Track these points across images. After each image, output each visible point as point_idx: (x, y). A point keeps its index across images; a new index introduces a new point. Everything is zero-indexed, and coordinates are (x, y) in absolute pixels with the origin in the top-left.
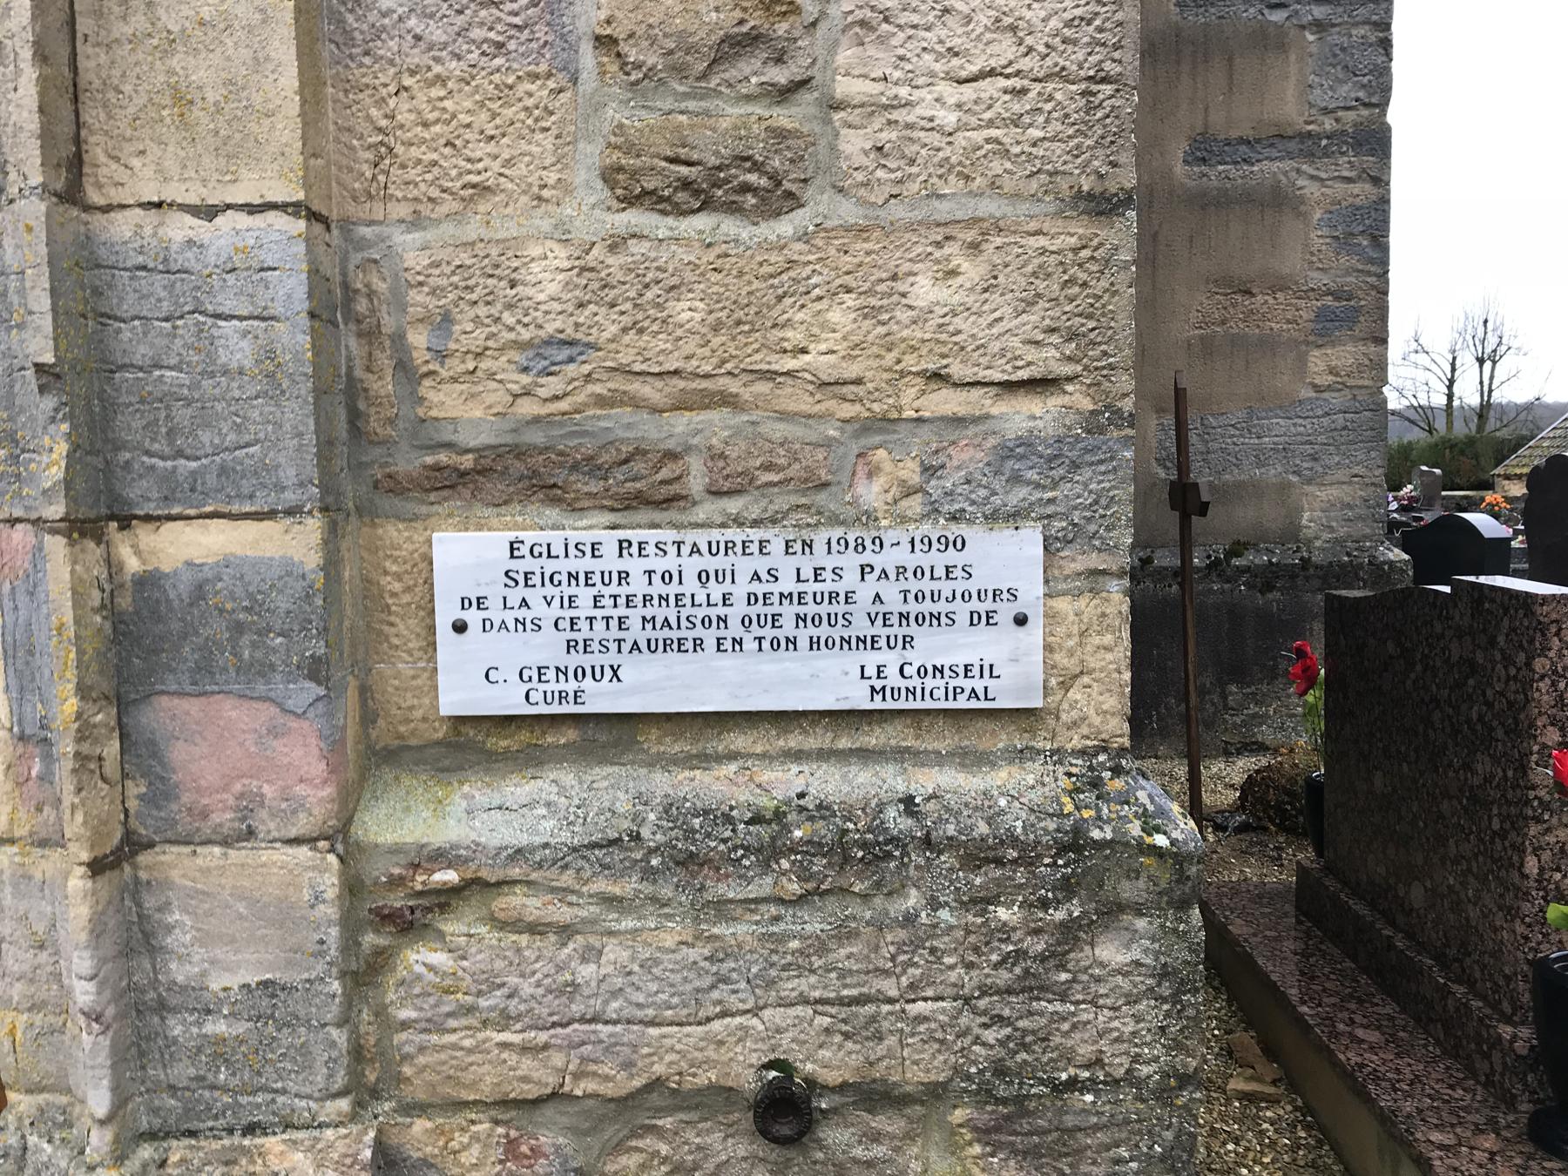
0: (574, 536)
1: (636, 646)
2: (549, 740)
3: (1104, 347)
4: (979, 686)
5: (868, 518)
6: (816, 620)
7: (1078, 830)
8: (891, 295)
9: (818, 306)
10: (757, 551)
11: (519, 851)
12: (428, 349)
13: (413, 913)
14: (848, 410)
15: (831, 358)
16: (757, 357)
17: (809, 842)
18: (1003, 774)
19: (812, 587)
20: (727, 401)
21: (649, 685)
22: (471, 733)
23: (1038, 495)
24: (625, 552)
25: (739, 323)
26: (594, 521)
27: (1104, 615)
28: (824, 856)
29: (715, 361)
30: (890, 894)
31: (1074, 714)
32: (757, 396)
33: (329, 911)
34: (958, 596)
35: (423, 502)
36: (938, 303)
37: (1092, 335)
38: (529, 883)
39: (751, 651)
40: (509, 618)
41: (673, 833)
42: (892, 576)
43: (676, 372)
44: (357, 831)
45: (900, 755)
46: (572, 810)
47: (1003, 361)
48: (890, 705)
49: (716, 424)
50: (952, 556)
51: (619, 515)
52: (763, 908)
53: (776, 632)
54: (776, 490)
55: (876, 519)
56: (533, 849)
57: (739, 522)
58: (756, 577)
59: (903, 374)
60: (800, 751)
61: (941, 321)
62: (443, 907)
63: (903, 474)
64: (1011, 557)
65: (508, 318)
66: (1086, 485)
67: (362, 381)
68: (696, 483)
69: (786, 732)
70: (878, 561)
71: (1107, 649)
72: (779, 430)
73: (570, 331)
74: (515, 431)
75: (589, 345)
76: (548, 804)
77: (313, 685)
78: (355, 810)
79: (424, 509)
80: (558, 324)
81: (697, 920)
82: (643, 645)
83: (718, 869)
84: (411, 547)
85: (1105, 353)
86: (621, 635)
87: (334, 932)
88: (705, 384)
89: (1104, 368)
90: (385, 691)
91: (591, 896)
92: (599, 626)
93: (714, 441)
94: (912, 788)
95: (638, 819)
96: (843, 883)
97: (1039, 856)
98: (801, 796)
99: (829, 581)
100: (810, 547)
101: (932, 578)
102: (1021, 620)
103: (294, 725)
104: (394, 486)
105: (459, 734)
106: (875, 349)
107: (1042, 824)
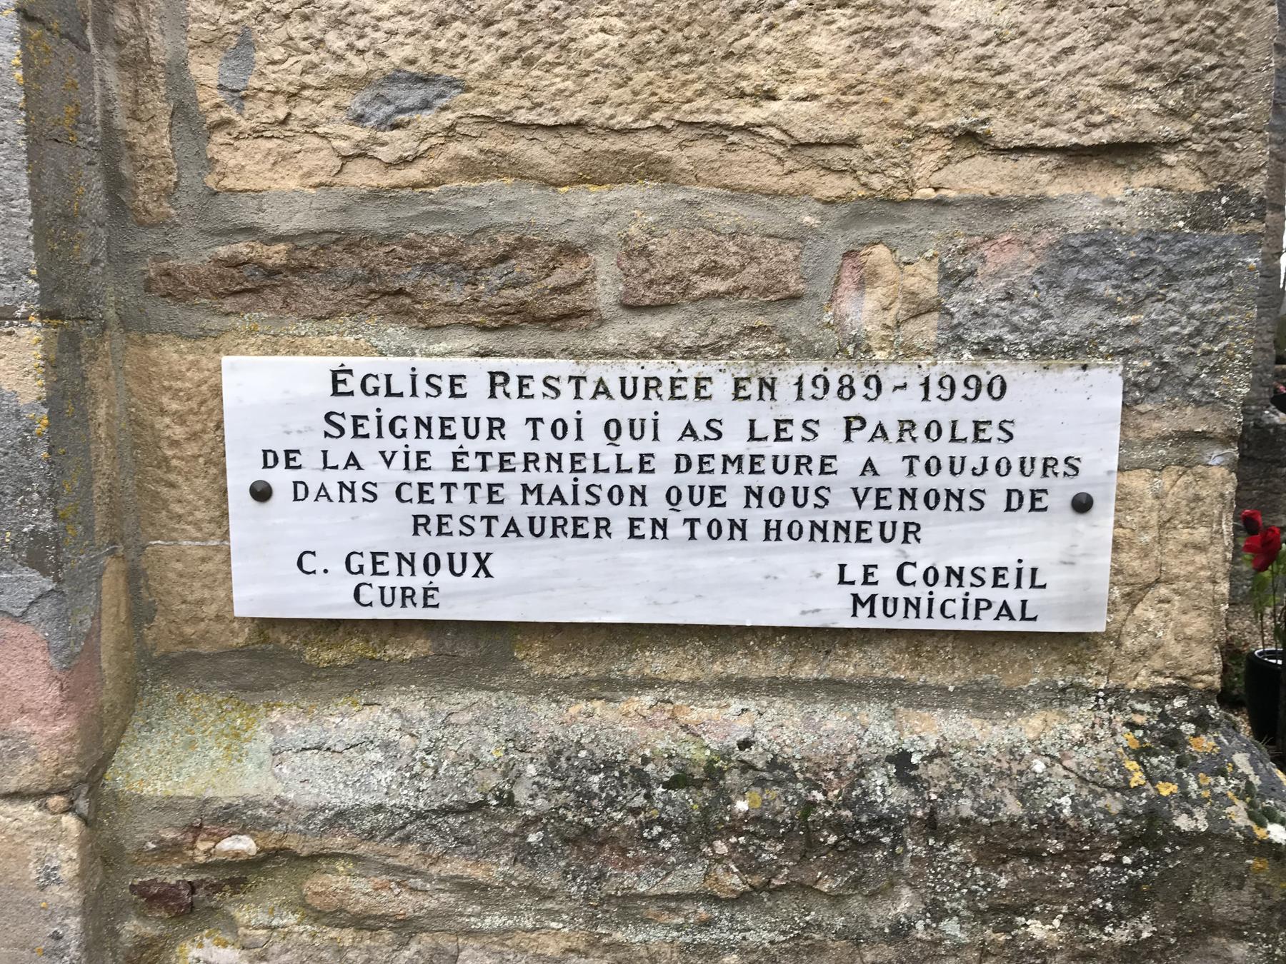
0: (425, 365)
1: (512, 527)
2: (391, 652)
3: (1226, 96)
4: (1013, 597)
5: (857, 347)
6: (776, 496)
7: (1155, 814)
8: (905, 11)
9: (795, 26)
10: (691, 394)
11: (341, 814)
12: (221, 87)
13: (193, 892)
14: (834, 186)
15: (812, 107)
16: (701, 103)
17: (758, 819)
18: (1036, 722)
19: (771, 448)
20: (653, 170)
21: (530, 583)
22: (283, 640)
23: (1111, 319)
24: (499, 390)
25: (675, 51)
26: (456, 345)
27: (1197, 498)
28: (779, 840)
29: (636, 108)
30: (873, 895)
31: (1144, 639)
32: (697, 163)
33: (66, 895)
34: (991, 466)
35: (214, 312)
36: (977, 24)
37: (1210, 78)
38: (356, 859)
39: (678, 538)
40: (331, 481)
41: (561, 798)
42: (893, 434)
43: (579, 125)
44: (116, 778)
45: (888, 691)
46: (419, 755)
47: (1072, 114)
48: (881, 622)
49: (636, 202)
50: (984, 407)
51: (493, 336)
52: (688, 907)
53: (715, 513)
54: (721, 304)
55: (869, 350)
56: (360, 813)
57: (665, 350)
58: (689, 431)
59: (918, 132)
60: (744, 680)
61: (981, 51)
62: (237, 885)
63: (912, 283)
64: (1074, 411)
65: (335, 41)
66: (1185, 305)
67: (124, 133)
68: (605, 293)
69: (725, 652)
70: (873, 412)
71: (1199, 548)
72: (731, 214)
73: (424, 61)
74: (344, 210)
75: (451, 83)
76: (386, 746)
77: (36, 575)
78: (116, 744)
79: (216, 322)
80: (408, 51)
81: (592, 920)
82: (523, 525)
83: (624, 851)
84: (197, 376)
85: (1228, 105)
86: (492, 510)
87: (74, 923)
88: (621, 144)
89: (1224, 127)
90: (163, 579)
91: (442, 880)
92: (461, 496)
93: (633, 230)
94: (907, 737)
95: (511, 773)
96: (803, 876)
97: (1096, 851)
98: (745, 744)
99: (797, 439)
100: (772, 388)
101: (953, 439)
102: (1082, 505)
103: (11, 631)
104: (173, 288)
105: (266, 640)
106: (878, 94)
107: (1101, 803)
